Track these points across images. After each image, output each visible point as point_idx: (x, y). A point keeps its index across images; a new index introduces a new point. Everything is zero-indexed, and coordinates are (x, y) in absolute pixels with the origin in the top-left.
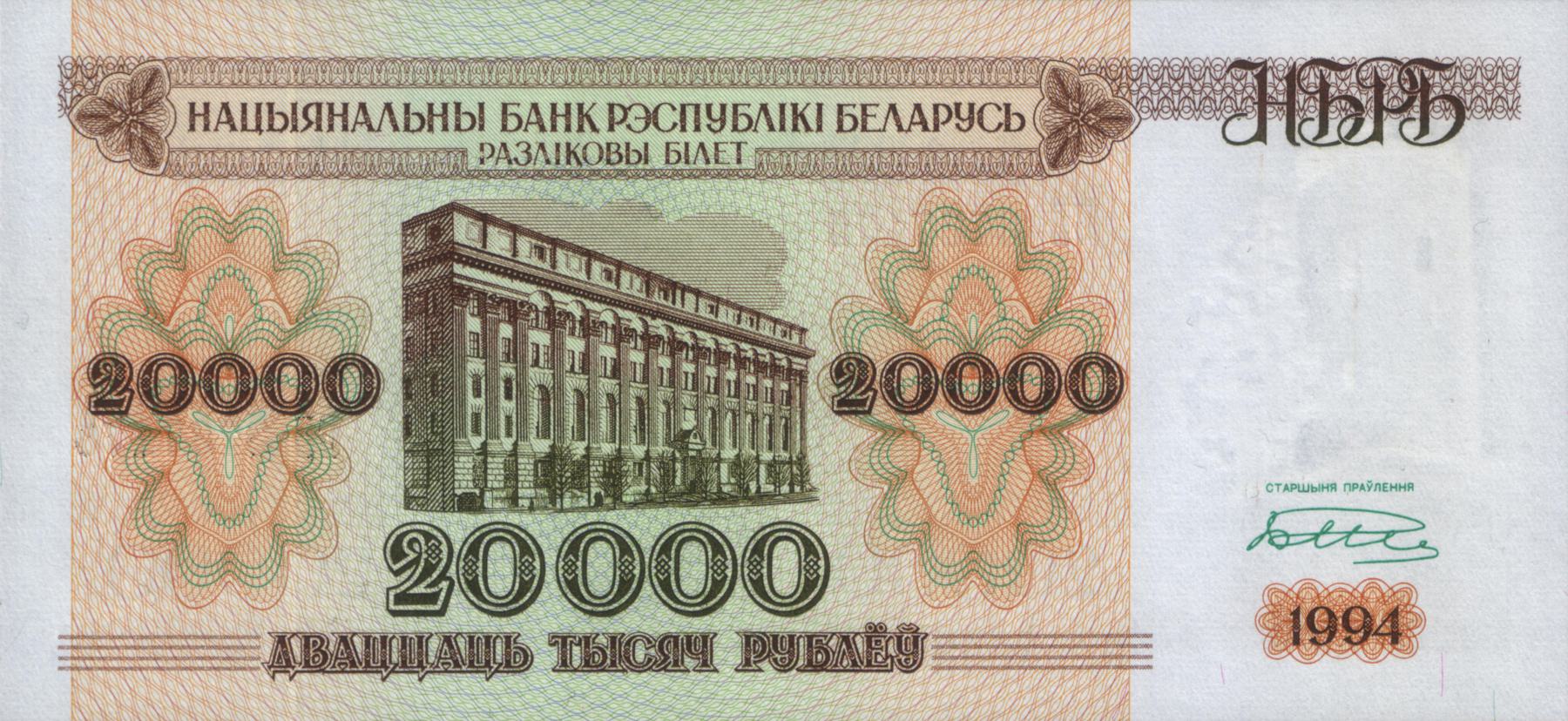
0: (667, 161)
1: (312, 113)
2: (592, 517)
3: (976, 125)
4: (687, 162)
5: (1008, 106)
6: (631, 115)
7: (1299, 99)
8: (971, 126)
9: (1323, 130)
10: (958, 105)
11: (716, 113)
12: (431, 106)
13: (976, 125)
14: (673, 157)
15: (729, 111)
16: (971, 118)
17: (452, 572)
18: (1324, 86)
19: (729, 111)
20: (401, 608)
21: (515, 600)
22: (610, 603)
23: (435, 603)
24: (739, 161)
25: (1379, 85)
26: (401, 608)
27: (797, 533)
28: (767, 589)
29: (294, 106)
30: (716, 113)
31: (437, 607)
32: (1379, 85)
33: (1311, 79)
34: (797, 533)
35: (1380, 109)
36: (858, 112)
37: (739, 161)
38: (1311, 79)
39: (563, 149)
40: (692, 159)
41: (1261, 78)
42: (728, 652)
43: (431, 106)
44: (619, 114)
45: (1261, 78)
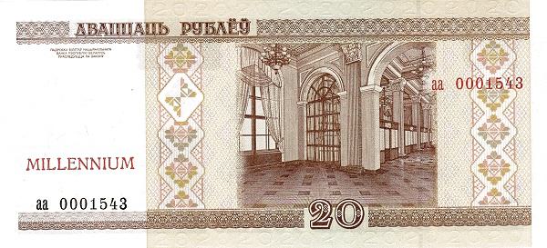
17: (332, 215)
21: (356, 222)
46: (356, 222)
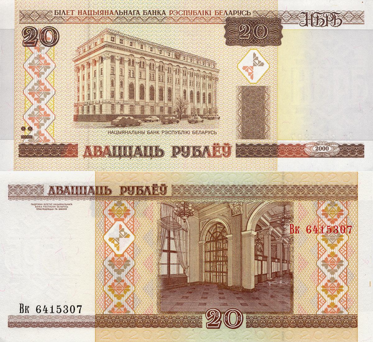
0: (216, 15)
1: (102, 12)
2: (47, 25)
3: (242, 14)
4: (60, 14)
5: (248, 11)
6: (174, 13)
7: (312, 19)
8: (177, 14)
9: (317, 24)
10: (238, 11)
11: (190, 12)
12: (124, 11)
13: (242, 14)
14: (217, 13)
15: (193, 12)
16: (241, 13)
18: (318, 17)
19: (193, 12)
20: (210, 327)
22: (230, 311)
23: (217, 326)
24: (72, 14)
25: (327, 17)
26: (210, 327)
27: (51, 29)
28: (45, 41)
29: (98, 11)
30: (190, 12)
31: (207, 324)
32: (327, 17)
33: (315, 15)
34: (51, 29)
35: (327, 20)
36: (219, 12)
37: (72, 14)
38: (315, 15)
39: (204, 12)
40: (61, 14)
41: (307, 15)
42: (43, 204)
43: (124, 11)
44: (171, 12)
45: (307, 15)
46: (54, 42)
